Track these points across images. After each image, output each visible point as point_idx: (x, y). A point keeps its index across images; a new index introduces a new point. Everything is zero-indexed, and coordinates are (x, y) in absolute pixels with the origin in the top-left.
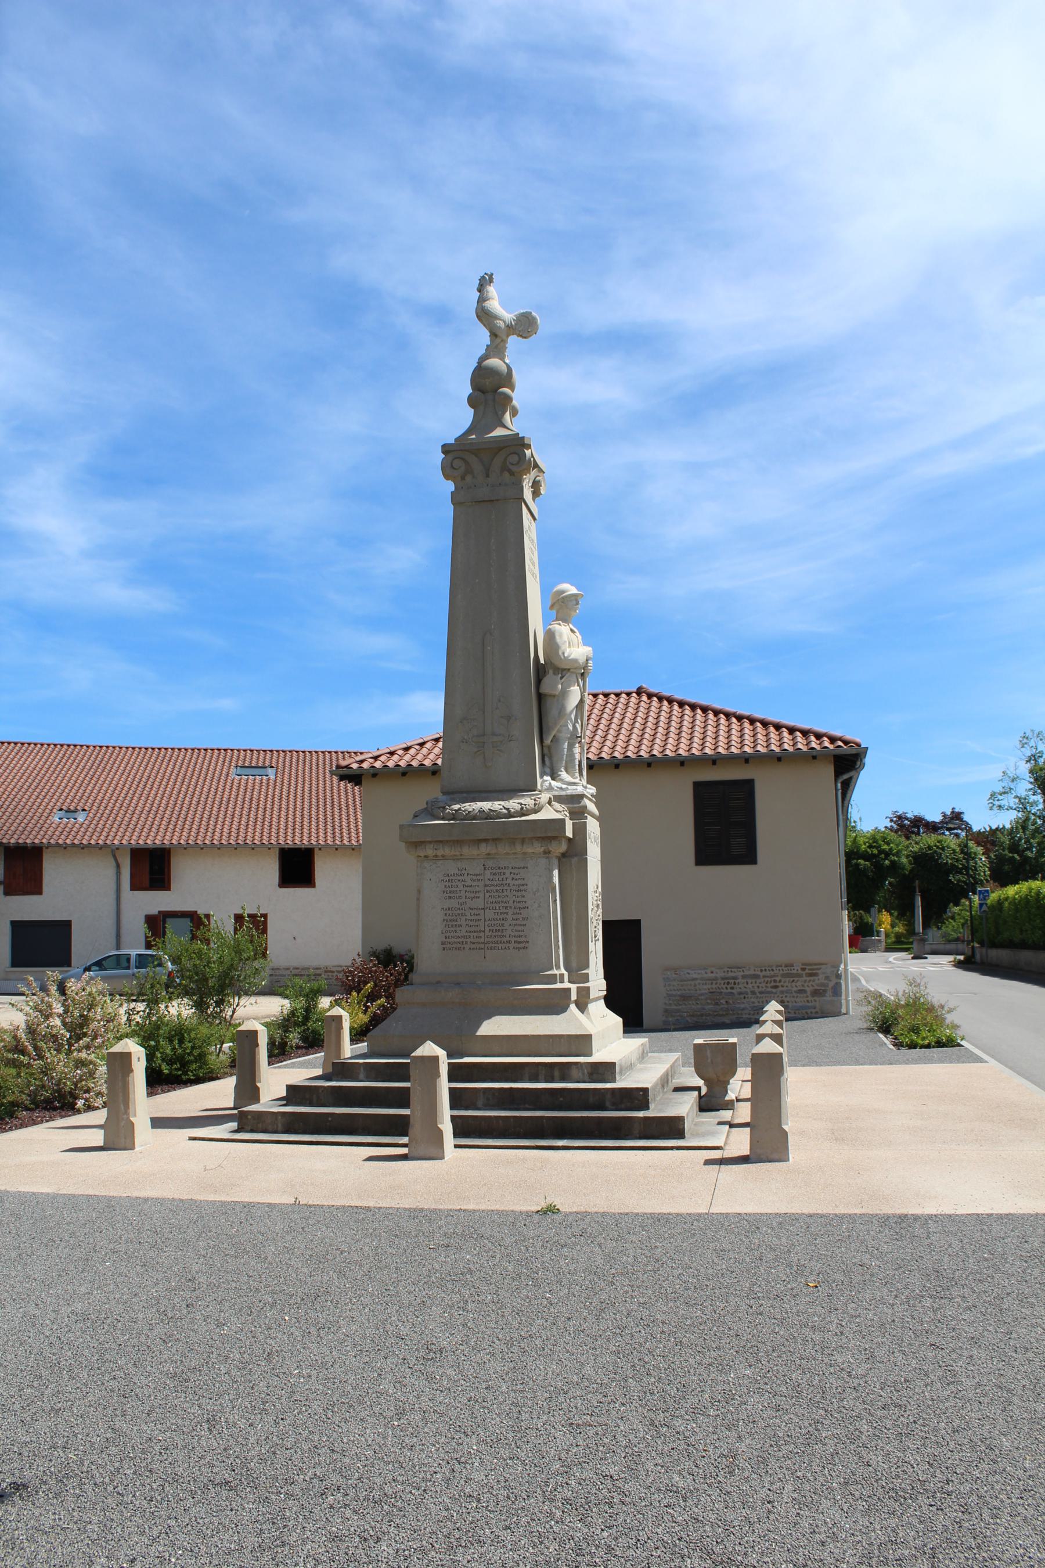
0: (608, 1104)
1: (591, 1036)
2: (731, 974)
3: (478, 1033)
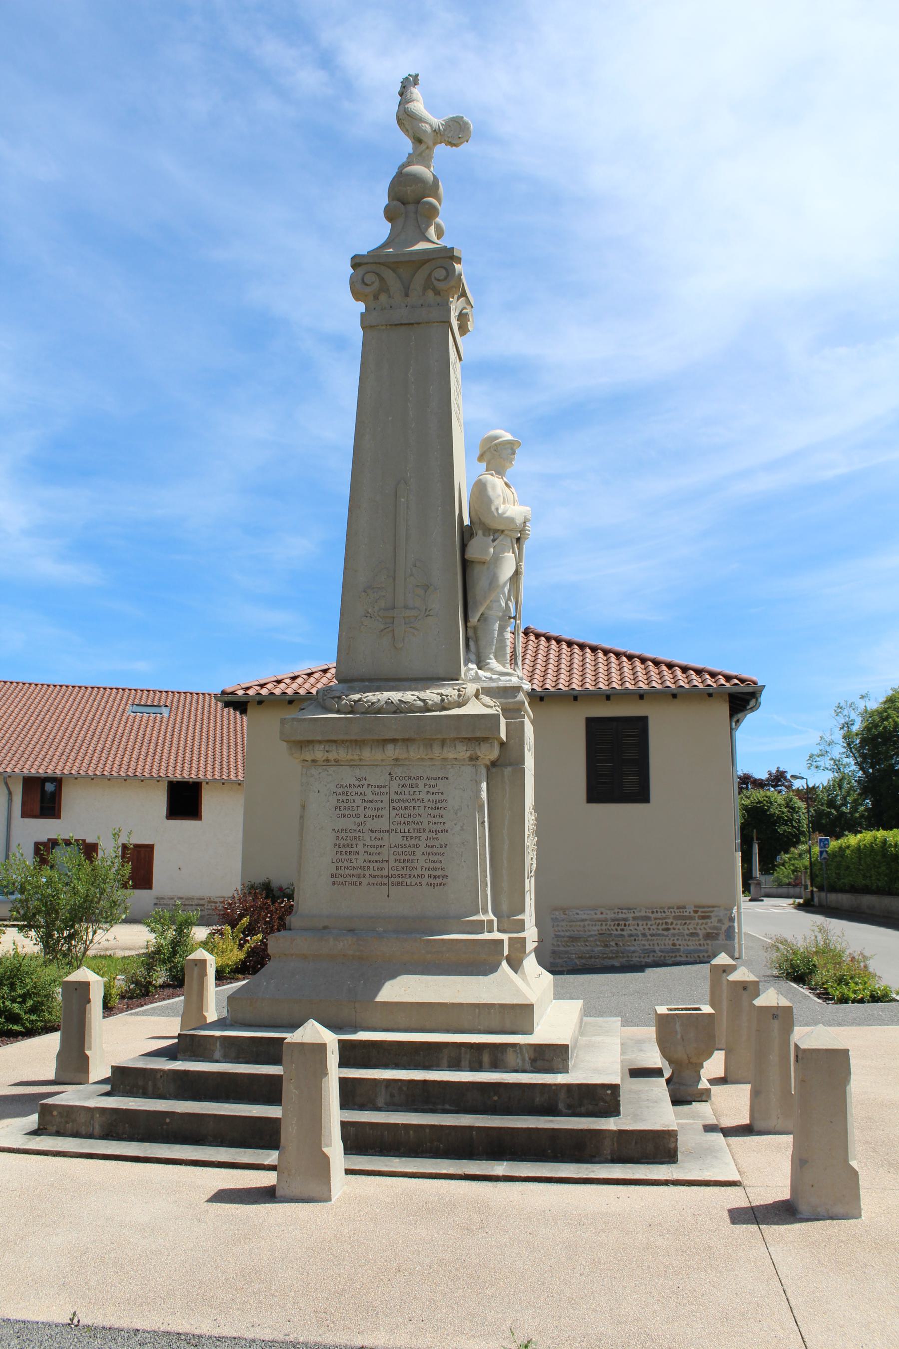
0: (561, 1106)
2: (621, 916)
3: (378, 999)
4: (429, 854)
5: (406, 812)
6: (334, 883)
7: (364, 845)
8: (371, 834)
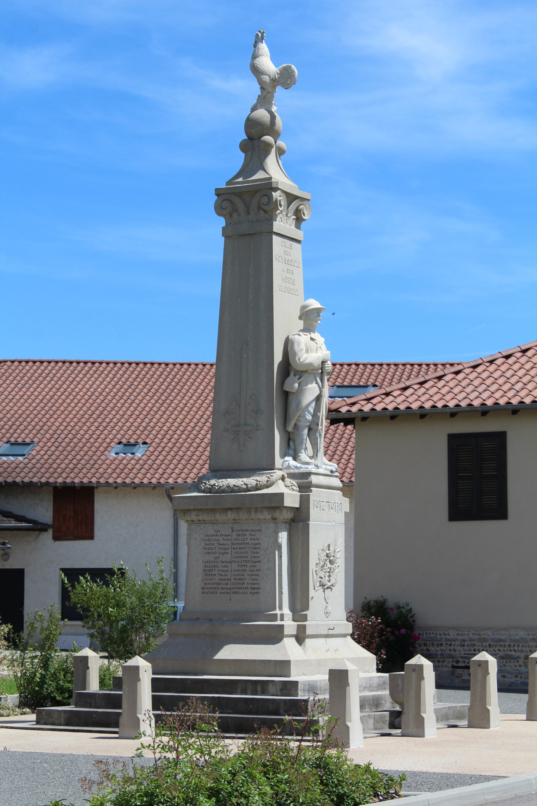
1: (290, 661)
3: (216, 657)
4: (251, 575)
5: (240, 550)
6: (203, 593)
7: (219, 570)
8: (222, 564)
